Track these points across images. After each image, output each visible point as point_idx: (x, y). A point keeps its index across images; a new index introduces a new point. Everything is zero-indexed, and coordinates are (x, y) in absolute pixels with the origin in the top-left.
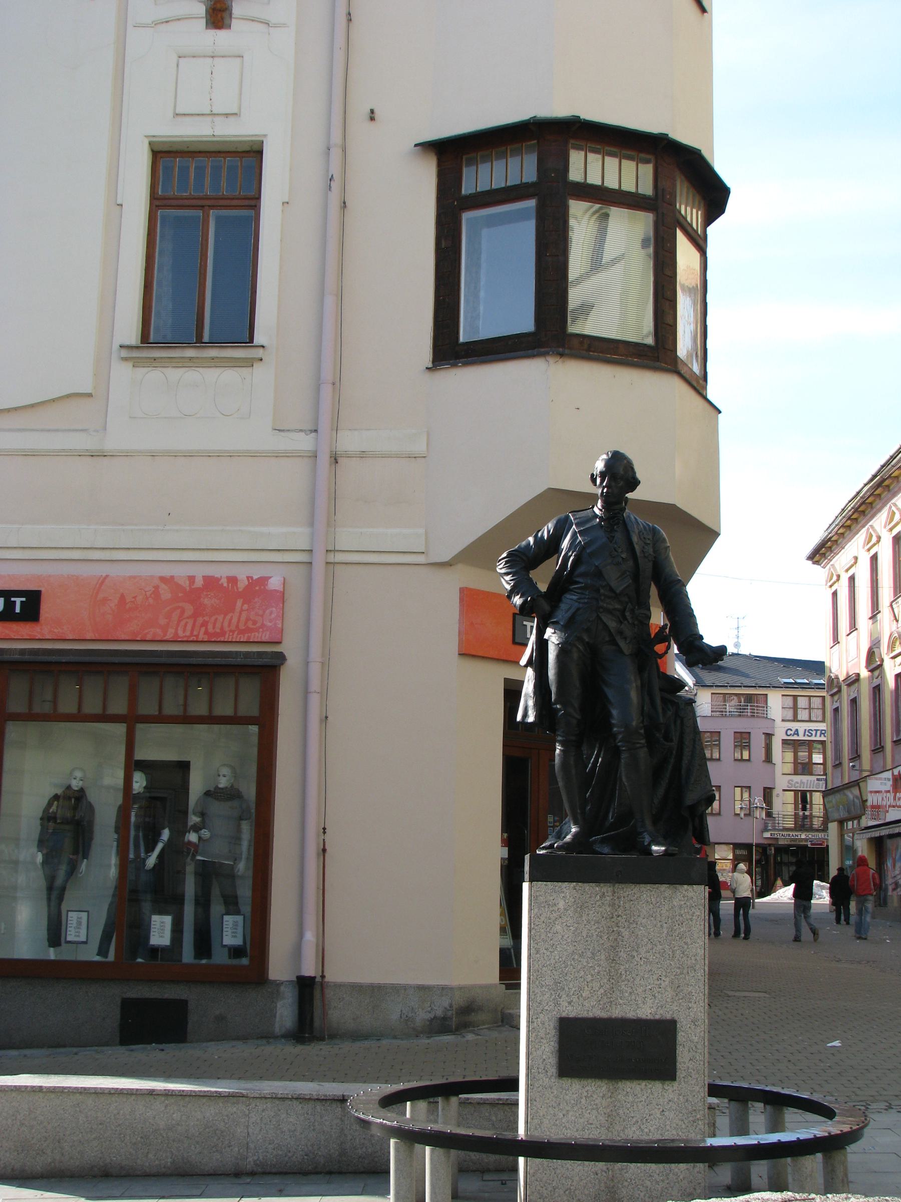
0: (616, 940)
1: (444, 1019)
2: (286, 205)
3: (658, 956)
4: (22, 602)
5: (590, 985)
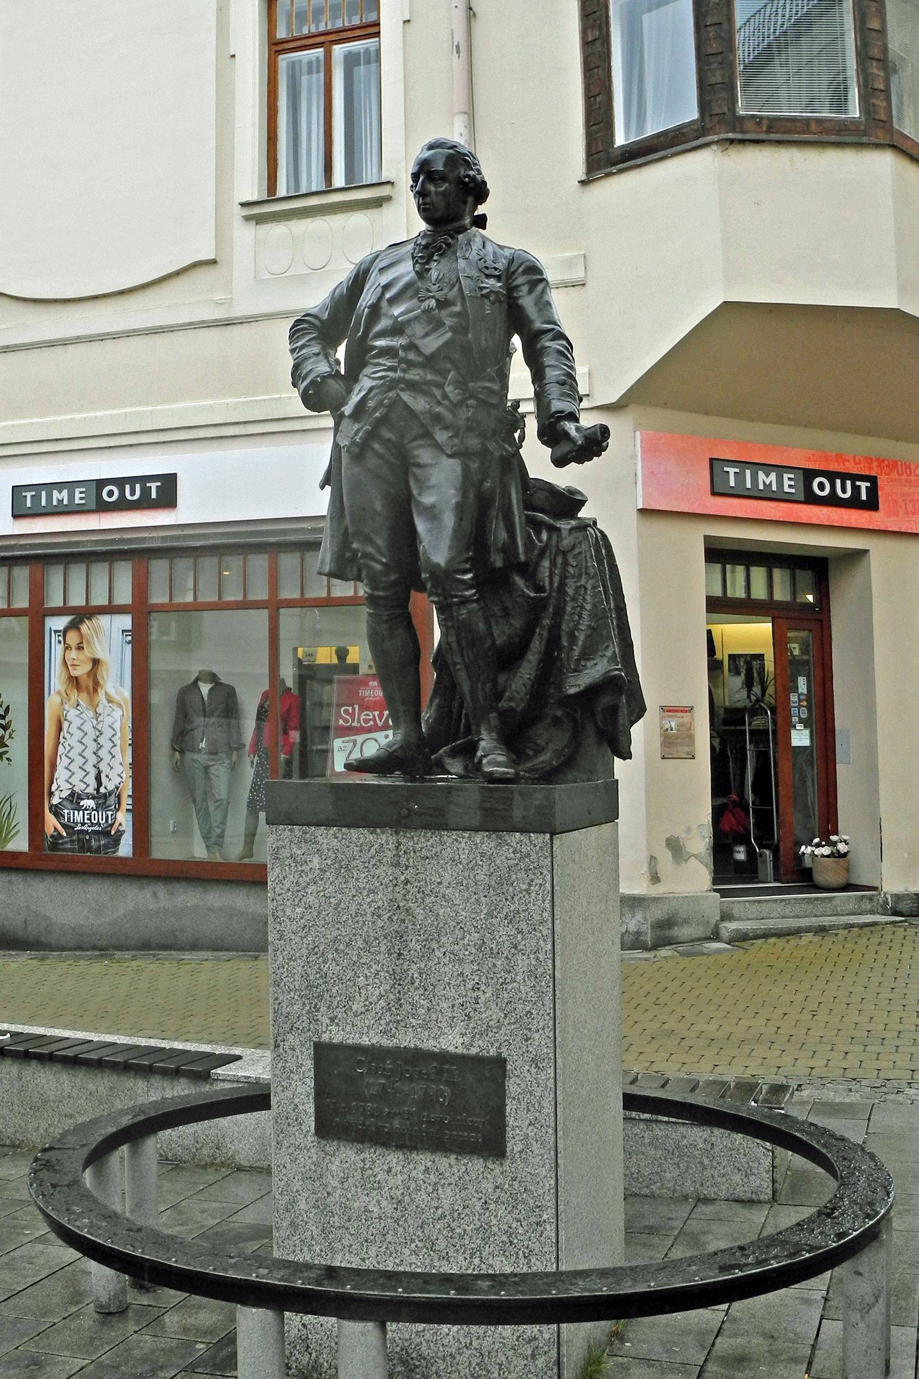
0: (403, 921)
1: (638, 933)
2: (407, 24)
3: (474, 951)
4: (157, 487)
5: (363, 992)
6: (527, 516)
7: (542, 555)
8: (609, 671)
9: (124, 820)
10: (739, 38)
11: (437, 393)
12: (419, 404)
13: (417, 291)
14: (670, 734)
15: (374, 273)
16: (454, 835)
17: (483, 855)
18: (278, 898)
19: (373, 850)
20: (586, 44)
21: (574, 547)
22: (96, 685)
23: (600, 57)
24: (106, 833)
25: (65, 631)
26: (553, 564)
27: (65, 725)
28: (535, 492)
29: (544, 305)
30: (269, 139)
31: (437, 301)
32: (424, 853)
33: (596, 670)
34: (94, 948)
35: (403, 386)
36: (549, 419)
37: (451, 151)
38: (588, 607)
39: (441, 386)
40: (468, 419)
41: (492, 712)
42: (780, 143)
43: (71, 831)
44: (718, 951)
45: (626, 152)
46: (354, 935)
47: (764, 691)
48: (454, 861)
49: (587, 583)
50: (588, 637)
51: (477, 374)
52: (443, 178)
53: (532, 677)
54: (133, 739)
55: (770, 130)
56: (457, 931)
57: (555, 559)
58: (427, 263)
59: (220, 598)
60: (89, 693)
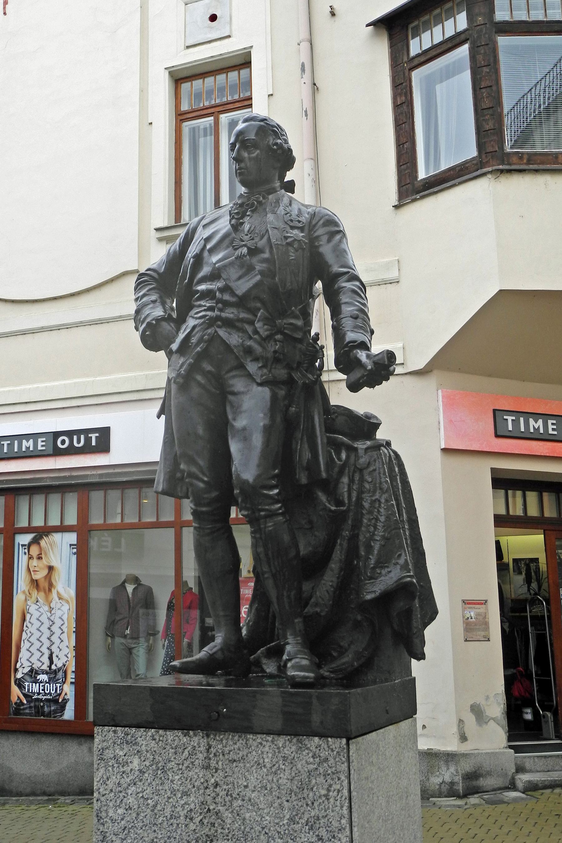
0: (213, 825)
1: (452, 783)
2: (271, 97)
4: (96, 437)
6: (328, 438)
7: (341, 473)
8: (401, 579)
9: (69, 690)
10: (507, 121)
11: (249, 329)
12: (234, 339)
13: (232, 242)
14: (470, 622)
15: (200, 228)
16: (259, 738)
17: (285, 758)
18: (103, 799)
19: (186, 752)
20: (396, 107)
21: (369, 464)
22: (51, 586)
23: (406, 115)
24: (55, 701)
25: (29, 545)
26: (352, 481)
27: (28, 617)
28: (337, 417)
29: (341, 253)
30: (176, 183)
31: (249, 249)
32: (232, 756)
33: (389, 578)
34: (44, 794)
35: (219, 323)
36: (344, 348)
37: (262, 123)
38: (382, 519)
39: (252, 323)
40: (275, 352)
41: (296, 618)
42: (537, 171)
43: (30, 699)
44: (515, 800)
45: (427, 183)
46: (169, 838)
47: (540, 587)
48: (259, 764)
49: (380, 497)
50: (383, 546)
51: (283, 314)
52: (255, 145)
53: (335, 585)
54: (76, 628)
55: (529, 162)
56: (262, 837)
57: (353, 476)
58: (242, 218)
59: (140, 520)
60: (45, 592)
